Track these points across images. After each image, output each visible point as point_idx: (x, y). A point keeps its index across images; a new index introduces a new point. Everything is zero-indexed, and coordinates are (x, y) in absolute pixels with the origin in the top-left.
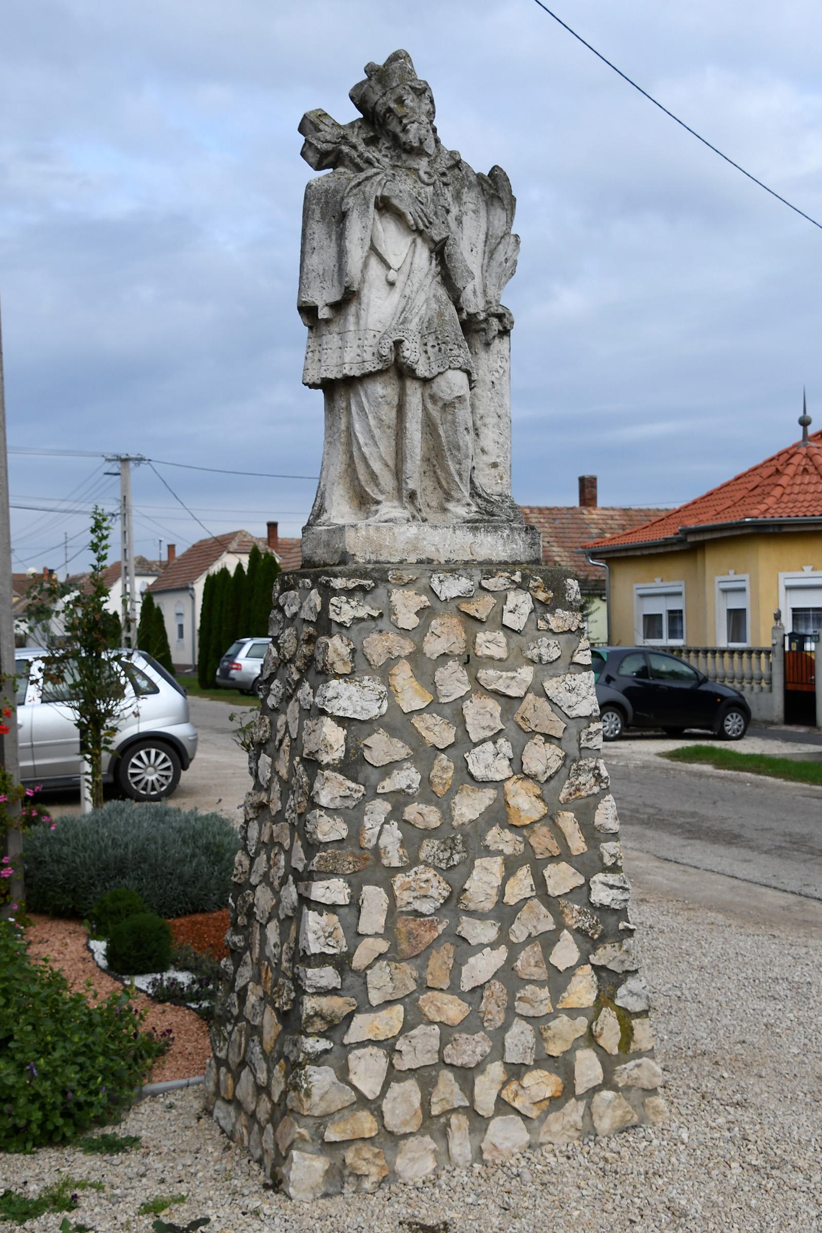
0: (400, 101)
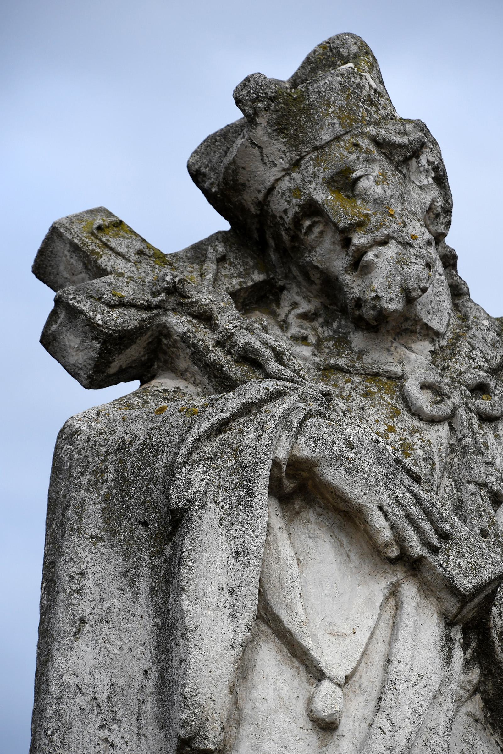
0: (344, 182)
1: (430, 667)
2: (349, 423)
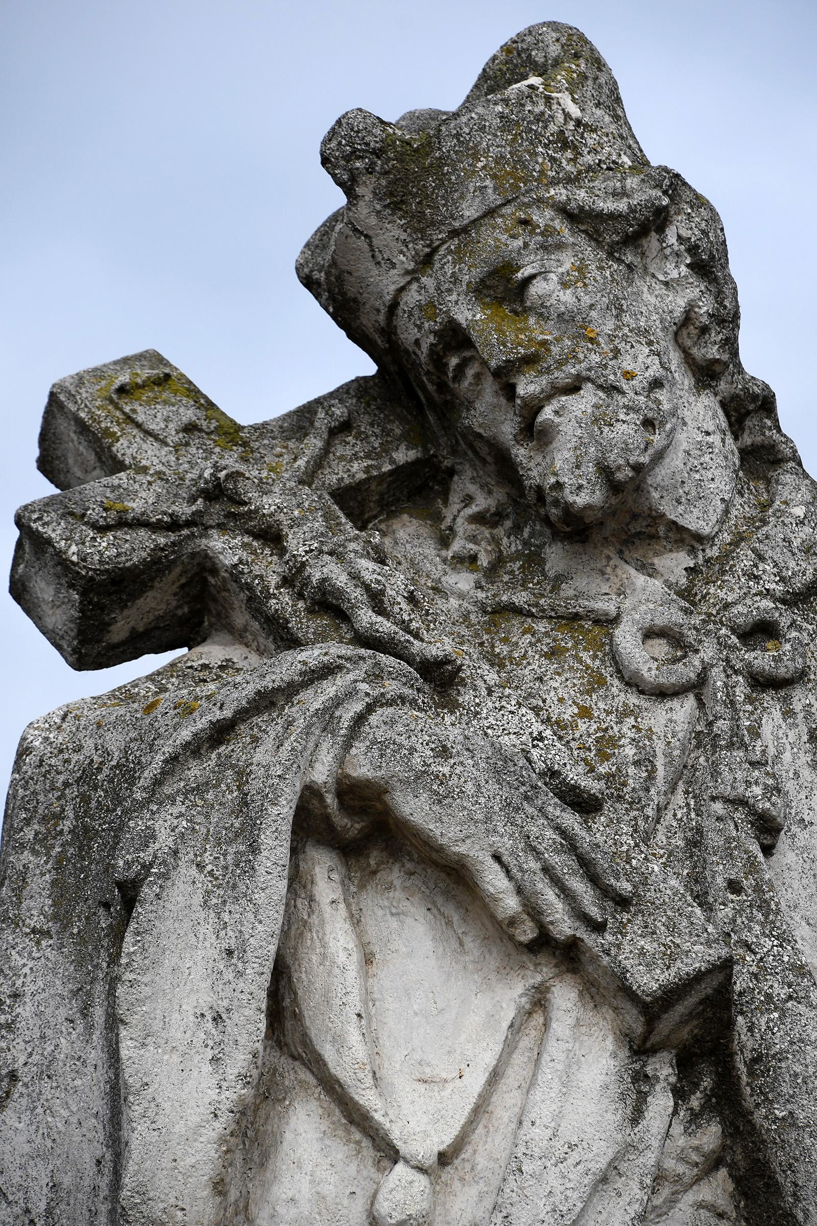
0: (505, 289)
1: (590, 1130)
2: (496, 708)
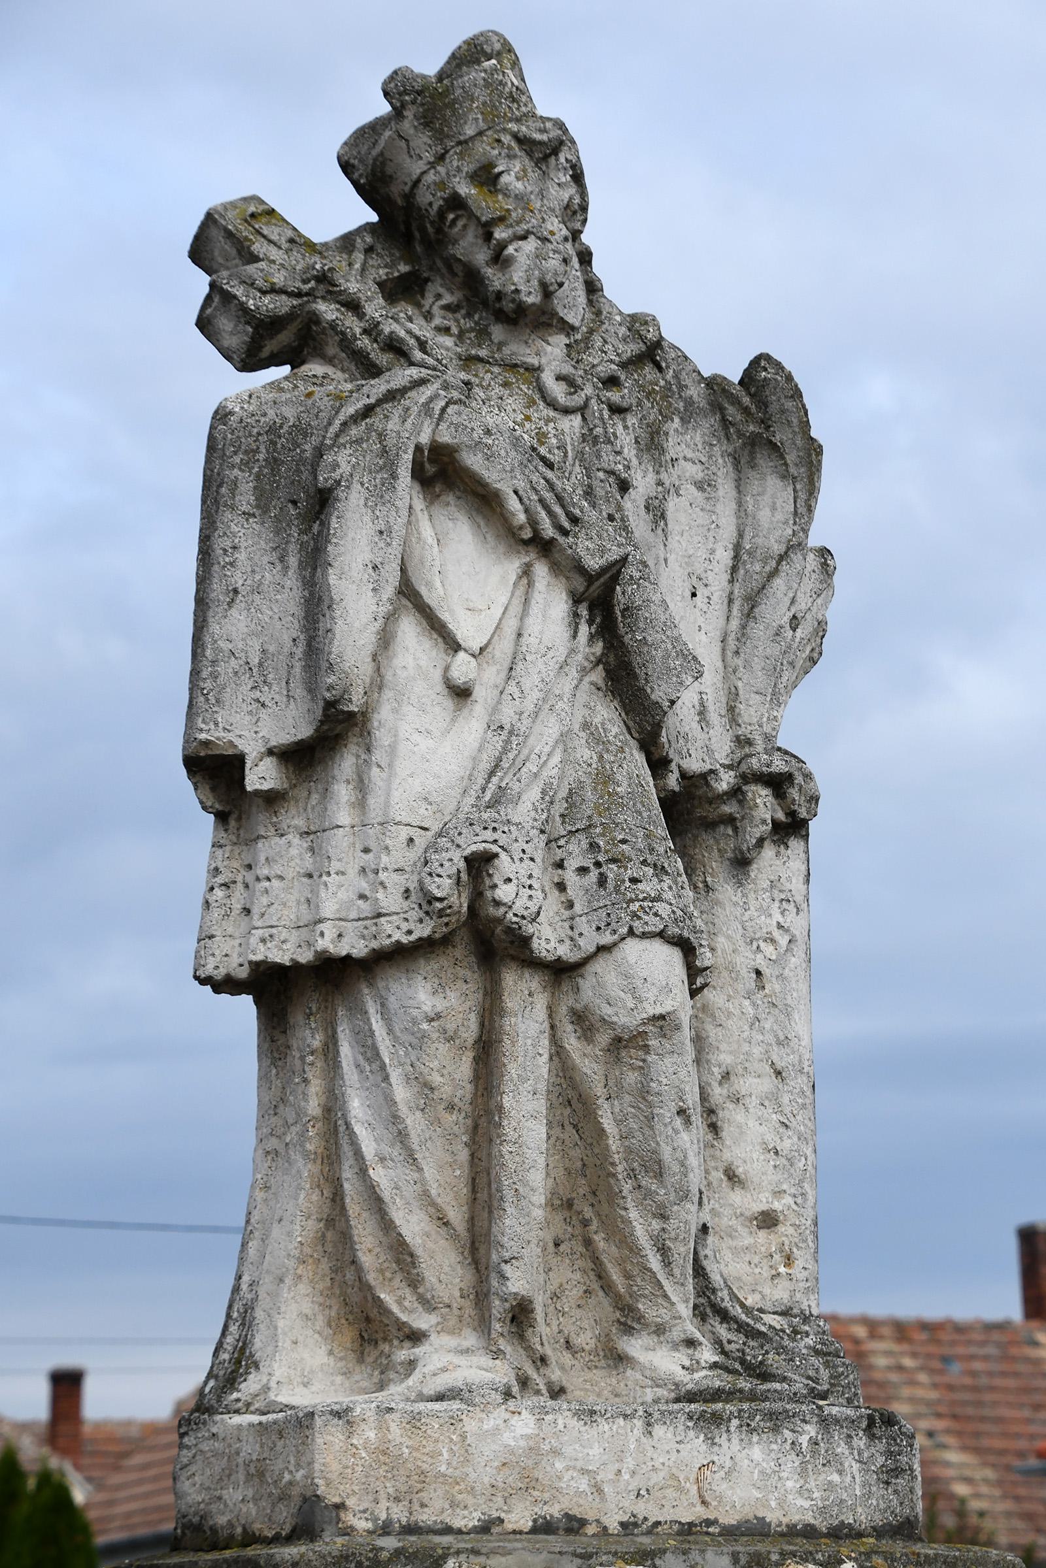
0: (487, 177)
